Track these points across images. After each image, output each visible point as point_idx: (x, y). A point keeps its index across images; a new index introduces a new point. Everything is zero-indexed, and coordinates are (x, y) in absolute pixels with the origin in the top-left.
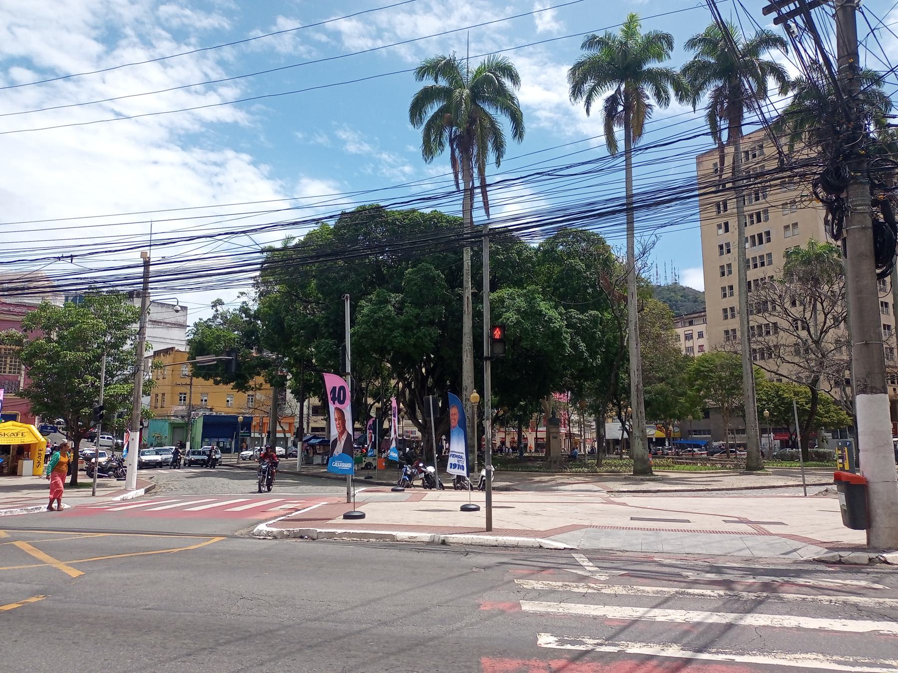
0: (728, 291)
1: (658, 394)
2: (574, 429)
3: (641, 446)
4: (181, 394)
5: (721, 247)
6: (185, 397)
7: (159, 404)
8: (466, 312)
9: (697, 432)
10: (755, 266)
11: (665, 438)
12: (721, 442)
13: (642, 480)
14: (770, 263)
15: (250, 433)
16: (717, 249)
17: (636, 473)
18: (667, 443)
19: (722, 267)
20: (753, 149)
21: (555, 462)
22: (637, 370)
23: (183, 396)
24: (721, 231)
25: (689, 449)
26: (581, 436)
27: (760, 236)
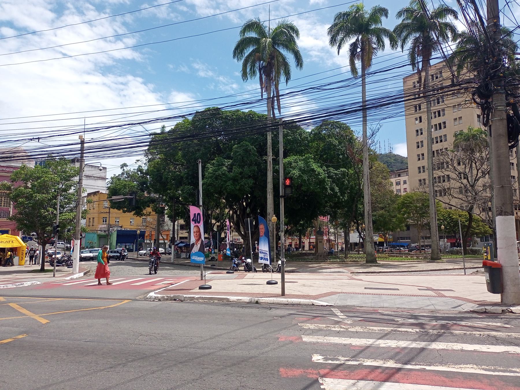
0: (421, 157)
1: (380, 217)
2: (332, 237)
3: (370, 246)
4: (104, 218)
5: (417, 131)
6: (106, 220)
7: (91, 224)
8: (269, 170)
9: (402, 238)
10: (437, 142)
11: (384, 242)
12: (416, 244)
13: (371, 266)
14: (446, 140)
15: (144, 240)
16: (415, 132)
17: (367, 262)
18: (385, 245)
19: (418, 143)
20: (436, 74)
21: (321, 256)
22: (368, 203)
23: (105, 219)
24: (417, 122)
25: (398, 248)
26: (335, 241)
27: (440, 124)
